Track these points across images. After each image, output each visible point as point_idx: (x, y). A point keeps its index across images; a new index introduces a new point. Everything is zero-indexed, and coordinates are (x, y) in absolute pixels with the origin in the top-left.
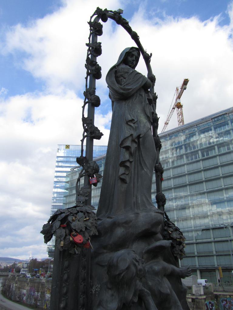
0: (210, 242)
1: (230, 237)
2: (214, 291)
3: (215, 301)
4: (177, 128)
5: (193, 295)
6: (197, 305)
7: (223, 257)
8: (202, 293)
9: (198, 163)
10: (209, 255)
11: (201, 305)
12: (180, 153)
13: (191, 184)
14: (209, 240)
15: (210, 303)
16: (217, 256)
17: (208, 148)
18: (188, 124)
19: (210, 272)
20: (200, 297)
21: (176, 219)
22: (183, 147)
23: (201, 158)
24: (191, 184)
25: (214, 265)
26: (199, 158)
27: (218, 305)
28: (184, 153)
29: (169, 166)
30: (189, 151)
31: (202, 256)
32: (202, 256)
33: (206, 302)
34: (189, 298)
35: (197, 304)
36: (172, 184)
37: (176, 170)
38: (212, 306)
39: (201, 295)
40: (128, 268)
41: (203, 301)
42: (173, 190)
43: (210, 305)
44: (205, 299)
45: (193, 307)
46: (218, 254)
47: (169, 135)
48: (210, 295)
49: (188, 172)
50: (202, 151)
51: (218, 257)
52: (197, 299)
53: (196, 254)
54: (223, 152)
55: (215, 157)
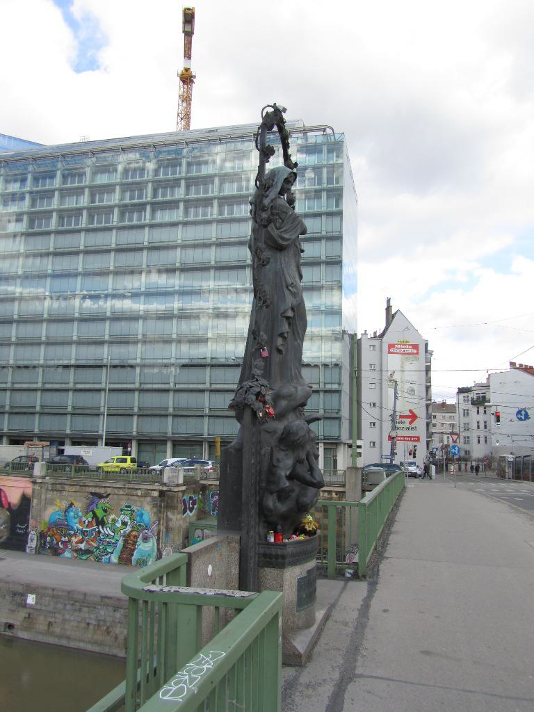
0: (202, 391)
1: (134, 383)
2: (201, 479)
3: (200, 496)
4: (171, 134)
5: (165, 484)
6: (167, 503)
7: (221, 420)
8: (181, 481)
9: (208, 227)
10: (29, 412)
11: (176, 502)
12: (220, 190)
13: (55, 276)
14: (166, 387)
15: (191, 498)
16: (139, 416)
17: (233, 197)
18: (201, 131)
19: (191, 445)
20: (176, 489)
21: (140, 337)
22: (183, 183)
23: (215, 216)
24: (55, 276)
25: (202, 434)
26: (211, 215)
27: (205, 504)
28: (182, 197)
29: (143, 219)
30: (127, 201)
31: (146, 415)
32: (146, 415)
33: (185, 497)
34: (154, 490)
35: (169, 501)
36: (178, 260)
37: (226, 227)
38: (194, 503)
39: (178, 485)
40: (304, 435)
41: (180, 494)
42: (212, 272)
43: (191, 501)
44: (184, 492)
45: (160, 506)
46: (212, 414)
47: (34, 159)
48: (194, 486)
49: (149, 243)
50: (32, 216)
51: (212, 420)
52: (170, 491)
53: (171, 410)
54: (191, 218)
55: (142, 227)
